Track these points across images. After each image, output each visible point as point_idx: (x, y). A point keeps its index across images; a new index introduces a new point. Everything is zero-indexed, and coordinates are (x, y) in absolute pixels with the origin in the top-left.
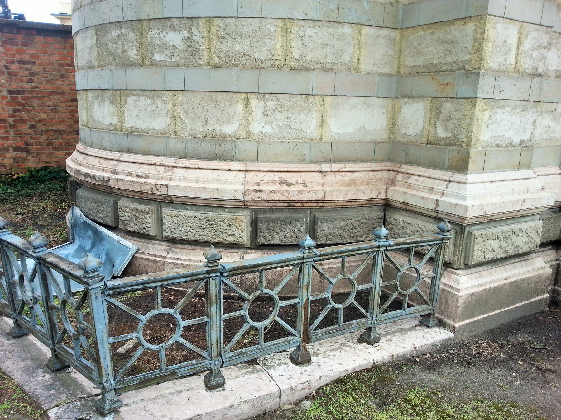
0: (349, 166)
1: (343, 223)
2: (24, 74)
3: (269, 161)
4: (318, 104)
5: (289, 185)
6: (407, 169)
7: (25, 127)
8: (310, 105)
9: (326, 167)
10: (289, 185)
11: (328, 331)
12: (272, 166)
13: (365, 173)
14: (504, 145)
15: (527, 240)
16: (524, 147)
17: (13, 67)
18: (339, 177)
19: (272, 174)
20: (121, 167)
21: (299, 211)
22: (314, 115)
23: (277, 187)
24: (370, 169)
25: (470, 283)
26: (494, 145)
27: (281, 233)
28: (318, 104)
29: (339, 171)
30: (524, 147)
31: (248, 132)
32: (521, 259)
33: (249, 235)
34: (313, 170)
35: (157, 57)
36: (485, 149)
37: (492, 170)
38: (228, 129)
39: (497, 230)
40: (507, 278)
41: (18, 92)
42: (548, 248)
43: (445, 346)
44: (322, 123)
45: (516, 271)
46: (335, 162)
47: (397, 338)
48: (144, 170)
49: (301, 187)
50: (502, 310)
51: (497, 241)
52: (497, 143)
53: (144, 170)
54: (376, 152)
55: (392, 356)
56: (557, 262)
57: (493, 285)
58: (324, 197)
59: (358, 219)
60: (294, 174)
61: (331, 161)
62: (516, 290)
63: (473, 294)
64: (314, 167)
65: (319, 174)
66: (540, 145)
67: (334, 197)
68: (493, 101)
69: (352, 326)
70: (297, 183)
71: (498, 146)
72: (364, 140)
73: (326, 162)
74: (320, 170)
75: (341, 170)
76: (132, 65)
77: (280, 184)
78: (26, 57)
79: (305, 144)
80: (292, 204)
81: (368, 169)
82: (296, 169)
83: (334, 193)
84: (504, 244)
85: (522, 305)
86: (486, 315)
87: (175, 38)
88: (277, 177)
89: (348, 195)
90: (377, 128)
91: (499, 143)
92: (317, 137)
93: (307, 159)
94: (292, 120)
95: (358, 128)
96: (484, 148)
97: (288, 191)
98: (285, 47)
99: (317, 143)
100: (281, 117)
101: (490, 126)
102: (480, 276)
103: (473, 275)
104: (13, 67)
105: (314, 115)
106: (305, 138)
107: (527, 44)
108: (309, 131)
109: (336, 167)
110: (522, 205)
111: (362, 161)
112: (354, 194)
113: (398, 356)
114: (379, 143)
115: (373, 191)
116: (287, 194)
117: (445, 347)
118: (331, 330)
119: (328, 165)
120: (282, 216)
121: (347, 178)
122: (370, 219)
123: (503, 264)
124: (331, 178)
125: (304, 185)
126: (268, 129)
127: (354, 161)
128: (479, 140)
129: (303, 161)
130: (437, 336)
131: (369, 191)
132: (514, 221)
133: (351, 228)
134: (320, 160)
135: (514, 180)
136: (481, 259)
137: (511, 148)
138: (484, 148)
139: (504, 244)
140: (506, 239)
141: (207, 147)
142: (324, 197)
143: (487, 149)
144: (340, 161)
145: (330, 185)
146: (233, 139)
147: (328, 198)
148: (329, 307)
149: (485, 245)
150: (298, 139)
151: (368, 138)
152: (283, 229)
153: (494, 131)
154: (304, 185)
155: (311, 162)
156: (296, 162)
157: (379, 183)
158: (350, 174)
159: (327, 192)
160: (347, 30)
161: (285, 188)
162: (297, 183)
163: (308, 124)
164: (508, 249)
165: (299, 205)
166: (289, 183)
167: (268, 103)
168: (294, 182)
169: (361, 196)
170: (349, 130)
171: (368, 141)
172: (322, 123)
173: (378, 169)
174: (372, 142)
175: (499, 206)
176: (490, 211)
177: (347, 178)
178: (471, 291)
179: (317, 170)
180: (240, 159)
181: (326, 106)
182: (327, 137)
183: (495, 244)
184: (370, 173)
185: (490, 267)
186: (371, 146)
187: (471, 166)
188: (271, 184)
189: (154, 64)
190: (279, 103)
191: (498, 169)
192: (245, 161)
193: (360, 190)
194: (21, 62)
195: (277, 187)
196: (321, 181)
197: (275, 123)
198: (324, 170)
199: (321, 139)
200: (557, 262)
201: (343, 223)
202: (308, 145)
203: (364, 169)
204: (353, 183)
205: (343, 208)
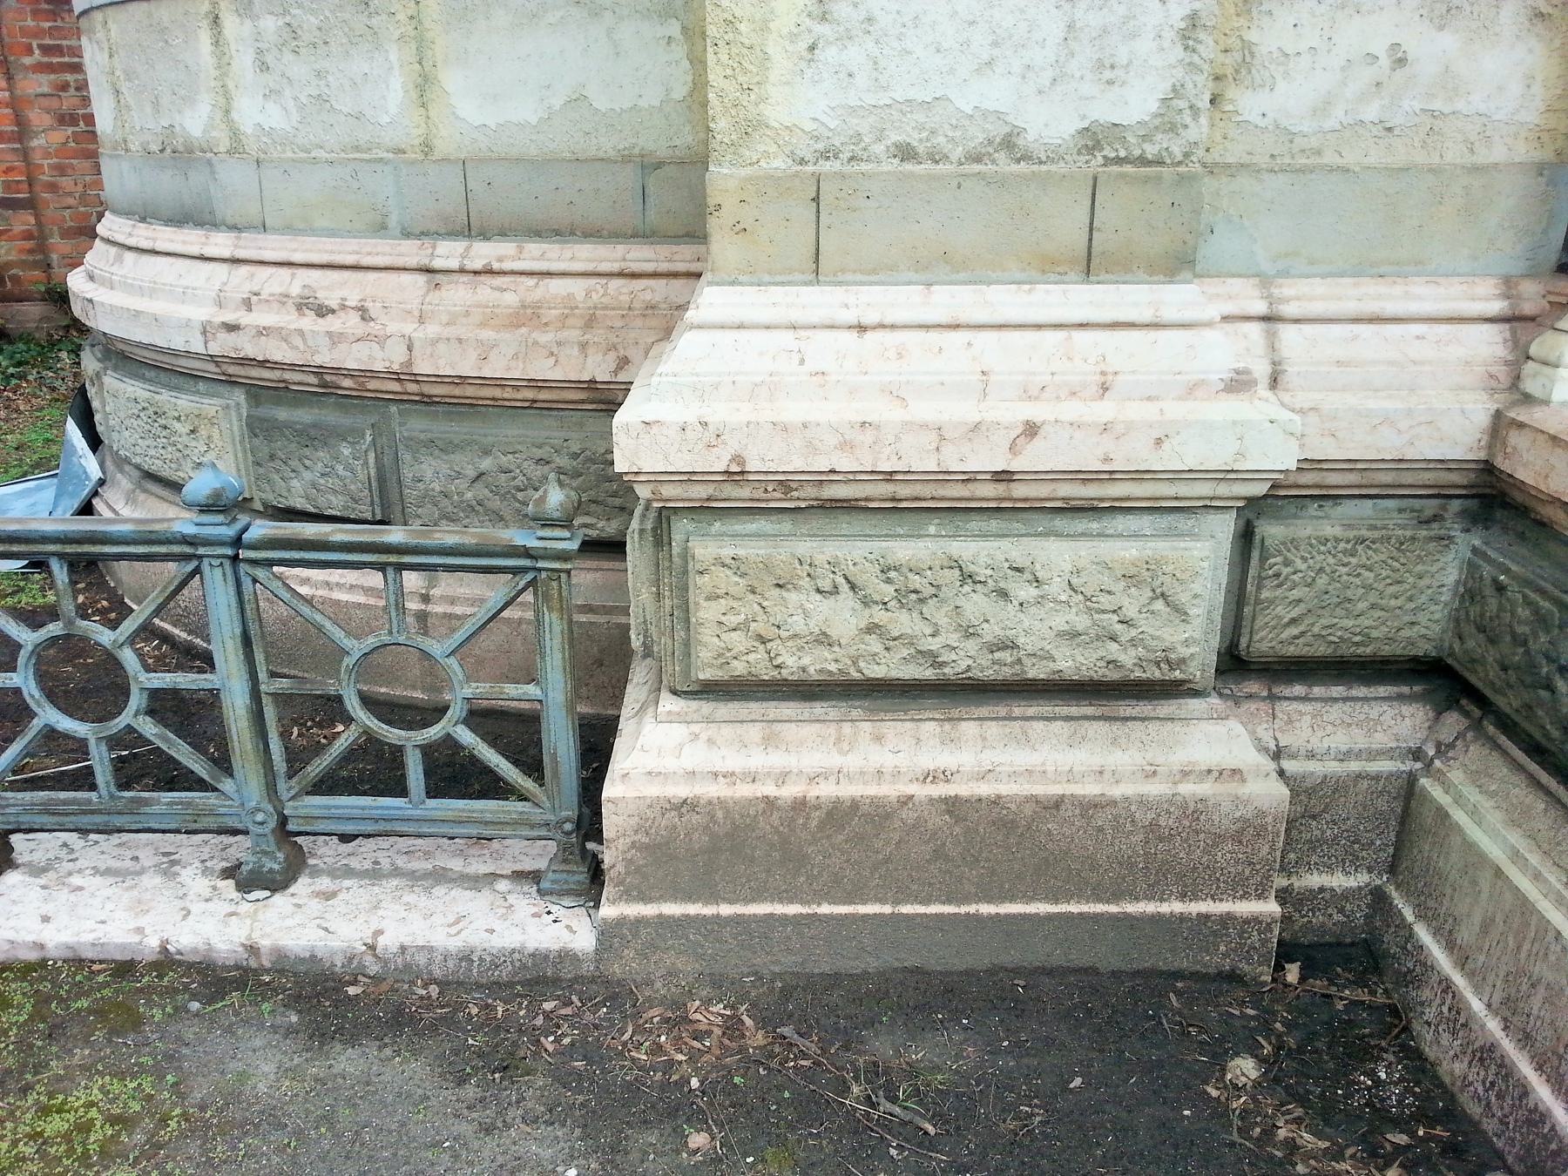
0: (536, 254)
1: (486, 464)
3: (289, 229)
4: (401, 16)
5: (322, 311)
6: (154, 240)
8: (374, 21)
9: (448, 253)
10: (322, 311)
11: (50, 802)
12: (294, 245)
13: (592, 281)
14: (958, 152)
15: (1082, 622)
16: (1108, 161)
18: (485, 292)
19: (285, 272)
22: (393, 57)
23: (287, 319)
24: (616, 267)
25: (698, 757)
26: (879, 149)
27: (307, 475)
28: (401, 16)
29: (490, 272)
30: (1108, 161)
31: (235, 134)
32: (1089, 711)
34: (400, 262)
36: (810, 168)
37: (878, 271)
38: (195, 122)
39: (855, 550)
40: (930, 777)
42: (1382, 690)
43: (538, 977)
44: (424, 86)
45: (1022, 758)
46: (485, 235)
47: (355, 893)
49: (354, 319)
50: (907, 909)
51: (846, 597)
52: (894, 137)
54: (651, 201)
55: (252, 950)
56: (1410, 765)
57: (826, 790)
58: (409, 363)
59: (539, 453)
60: (346, 274)
61: (469, 230)
62: (1172, 844)
63: (685, 806)
64: (410, 252)
65: (421, 279)
66: (1329, 158)
67: (442, 362)
69: (147, 810)
70: (343, 307)
71: (906, 153)
72: (592, 152)
73: (453, 234)
74: (425, 261)
75: (496, 266)
77: (299, 307)
79: (379, 167)
80: (328, 378)
81: (605, 267)
82: (350, 260)
83: (442, 347)
84: (903, 622)
85: (1050, 917)
86: (793, 909)
88: (296, 283)
89: (493, 356)
90: (642, 103)
91: (914, 138)
92: (416, 142)
93: (393, 221)
94: (330, 78)
95: (557, 103)
96: (802, 162)
97: (301, 332)
99: (413, 162)
100: (299, 69)
101: (829, 54)
102: (768, 741)
103: (727, 730)
105: (393, 57)
106: (379, 146)
108: (385, 119)
109: (483, 252)
110: (1013, 448)
111: (592, 234)
112: (515, 356)
113: (280, 955)
114: (659, 165)
115: (590, 351)
116: (298, 341)
117: (460, 983)
118: (65, 802)
119: (458, 246)
120: (304, 415)
121: (510, 296)
122: (589, 460)
123: (955, 713)
124: (457, 294)
125: (364, 314)
126: (275, 118)
127: (558, 233)
128: (761, 124)
129: (380, 229)
130: (568, 931)
131: (575, 351)
132: (1017, 526)
133: (517, 482)
134: (433, 228)
135: (1039, 327)
136: (751, 663)
137: (1015, 168)
138: (802, 162)
139: (903, 622)
140: (912, 599)
142: (409, 363)
143: (826, 167)
144: (503, 233)
145: (445, 318)
147: (423, 367)
148: (149, 728)
149: (741, 597)
150: (357, 149)
151: (608, 144)
152: (307, 462)
153: (861, 80)
154: (364, 314)
155: (407, 234)
156: (351, 234)
157: (639, 322)
158: (531, 282)
159: (417, 345)
161: (309, 322)
162: (343, 307)
163: (381, 96)
164: (934, 644)
165: (347, 383)
166: (320, 306)
167: (262, 23)
168: (334, 304)
169: (543, 369)
170: (525, 110)
171: (612, 153)
172: (424, 86)
173: (649, 267)
174: (626, 159)
175: (832, 440)
176: (770, 457)
177: (510, 296)
178: (682, 791)
179: (413, 262)
180: (230, 221)
181: (427, 24)
182: (447, 142)
183: (843, 616)
184: (616, 283)
185: (833, 713)
186: (628, 177)
187: (723, 248)
188: (275, 305)
190: (288, 19)
191: (920, 266)
193: (536, 343)
195: (287, 319)
196: (414, 306)
197: (287, 93)
198: (438, 263)
199: (427, 147)
200: (1410, 765)
201: (486, 464)
202: (387, 169)
203: (590, 267)
204: (527, 316)
205: (497, 405)
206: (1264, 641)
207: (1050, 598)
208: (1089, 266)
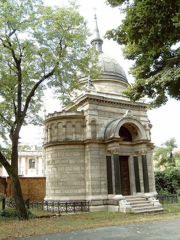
2: (31, 186)
7: (30, 196)
9: (78, 196)
17: (29, 185)
20: (55, 198)
21: (43, 166)
33: (97, 84)
35: (59, 185)
41: (30, 189)
44: (77, 191)
48: (58, 198)
53: (58, 198)
68: (148, 166)
76: (56, 186)
78: (31, 183)
87: (61, 183)
98: (73, 184)
100: (73, 191)
104: (29, 185)
107: (97, 182)
109: (79, 196)
141: (65, 195)
146: (68, 194)
160: (79, 181)
163: (76, 191)
172: (77, 191)
182: (78, 193)
189: (59, 186)
192: (131, 213)
194: (30, 184)
206: (104, 204)
207: (99, 202)
208: (99, 195)
